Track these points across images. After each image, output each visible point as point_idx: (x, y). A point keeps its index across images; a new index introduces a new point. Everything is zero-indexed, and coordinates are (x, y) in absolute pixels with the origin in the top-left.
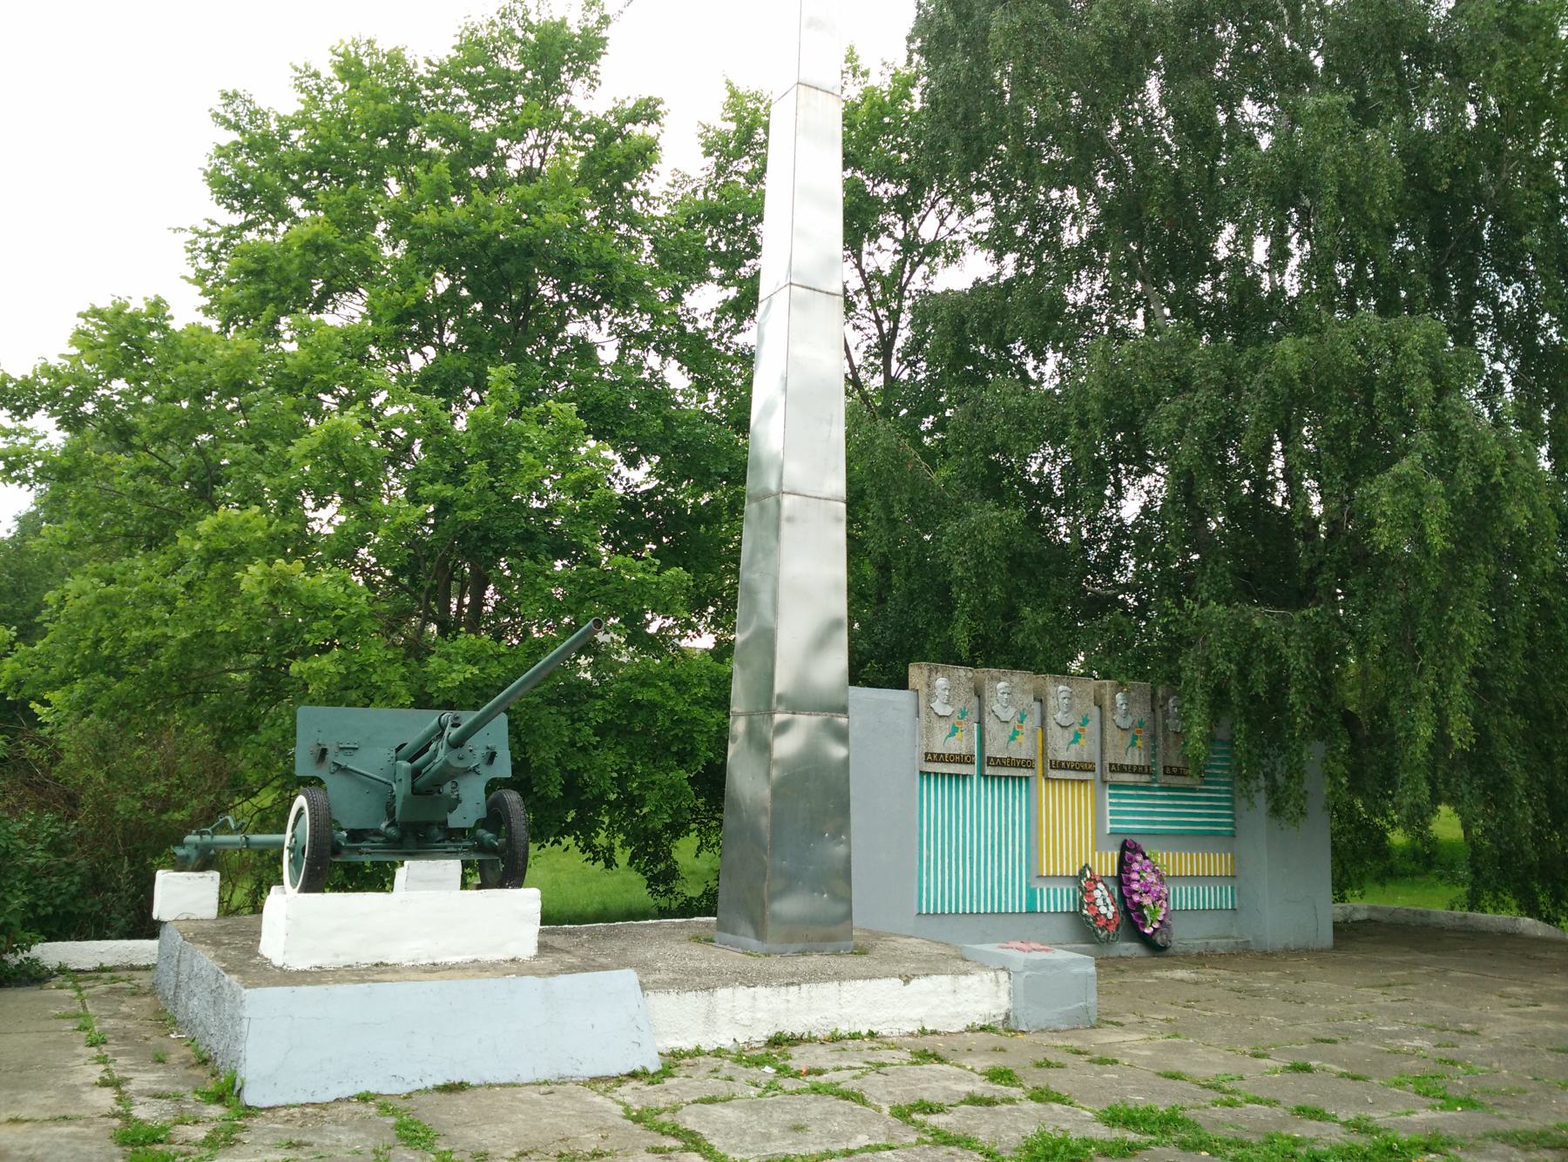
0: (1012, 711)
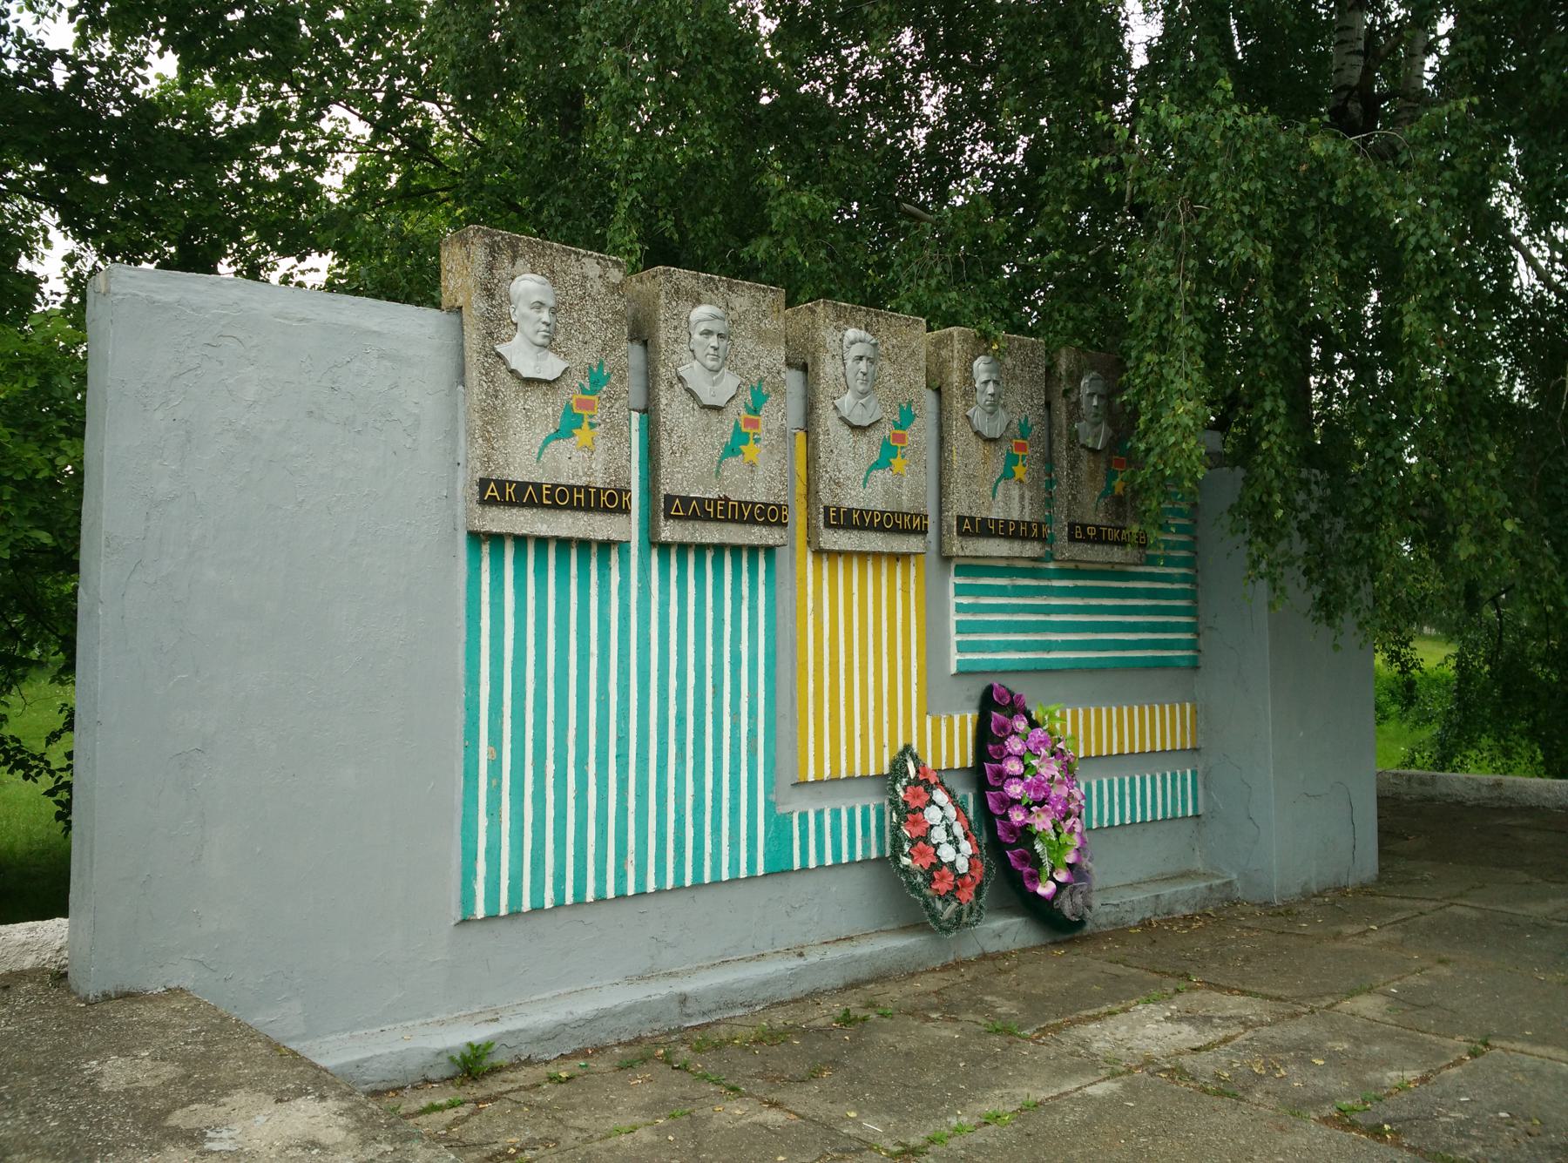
0: (729, 383)
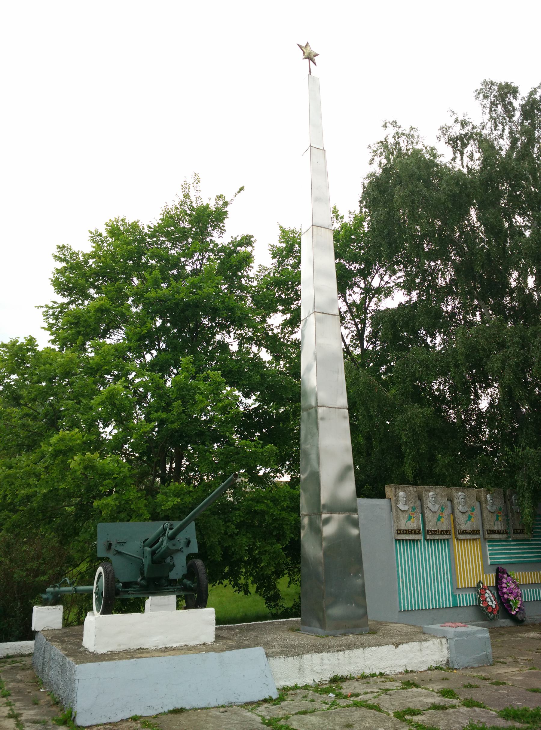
0: (437, 506)
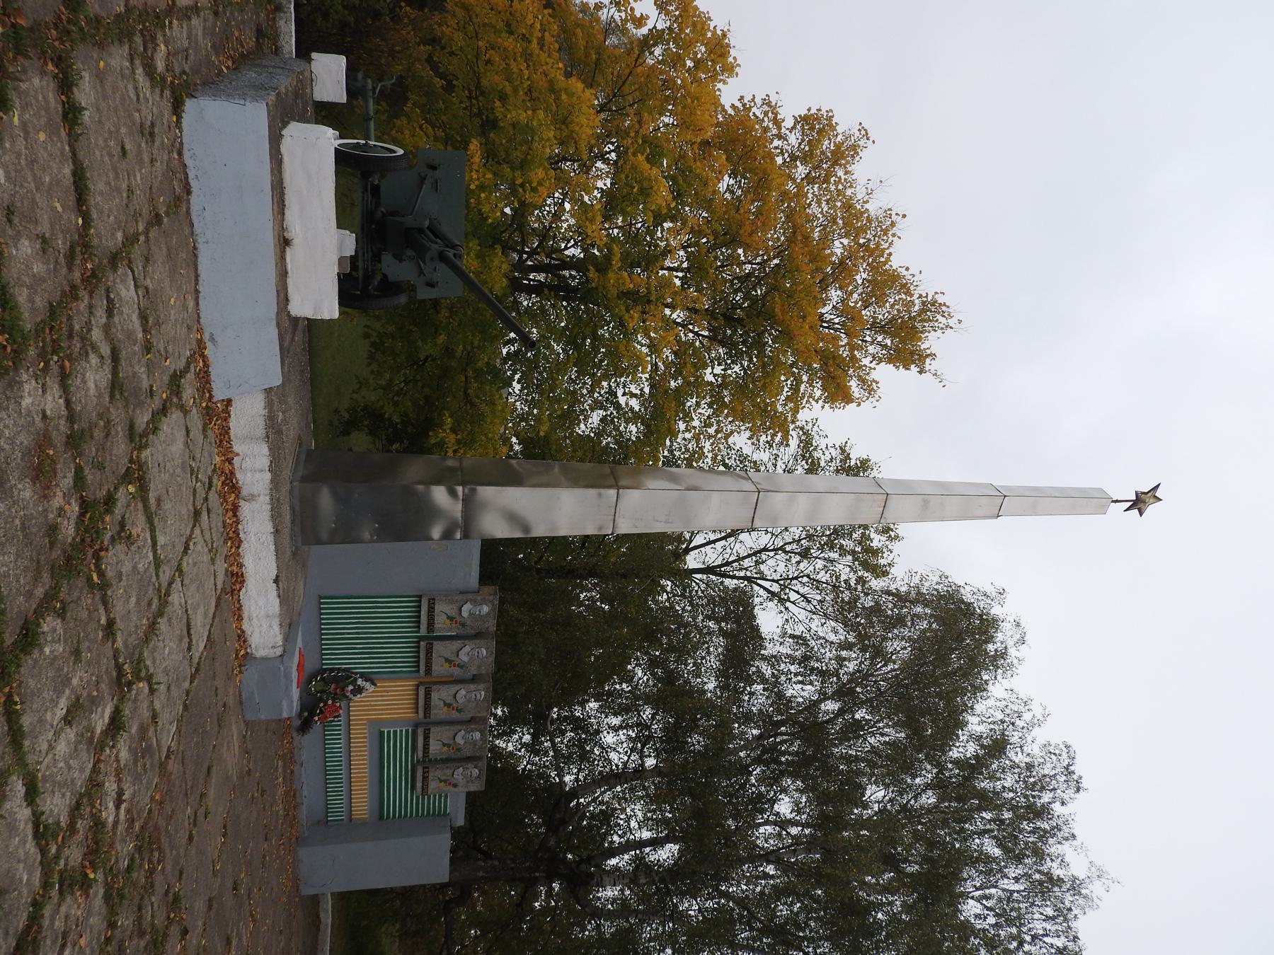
0: (465, 659)
